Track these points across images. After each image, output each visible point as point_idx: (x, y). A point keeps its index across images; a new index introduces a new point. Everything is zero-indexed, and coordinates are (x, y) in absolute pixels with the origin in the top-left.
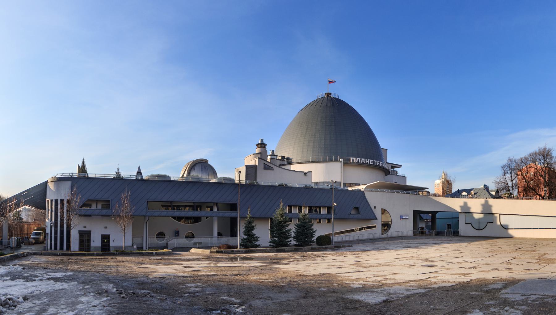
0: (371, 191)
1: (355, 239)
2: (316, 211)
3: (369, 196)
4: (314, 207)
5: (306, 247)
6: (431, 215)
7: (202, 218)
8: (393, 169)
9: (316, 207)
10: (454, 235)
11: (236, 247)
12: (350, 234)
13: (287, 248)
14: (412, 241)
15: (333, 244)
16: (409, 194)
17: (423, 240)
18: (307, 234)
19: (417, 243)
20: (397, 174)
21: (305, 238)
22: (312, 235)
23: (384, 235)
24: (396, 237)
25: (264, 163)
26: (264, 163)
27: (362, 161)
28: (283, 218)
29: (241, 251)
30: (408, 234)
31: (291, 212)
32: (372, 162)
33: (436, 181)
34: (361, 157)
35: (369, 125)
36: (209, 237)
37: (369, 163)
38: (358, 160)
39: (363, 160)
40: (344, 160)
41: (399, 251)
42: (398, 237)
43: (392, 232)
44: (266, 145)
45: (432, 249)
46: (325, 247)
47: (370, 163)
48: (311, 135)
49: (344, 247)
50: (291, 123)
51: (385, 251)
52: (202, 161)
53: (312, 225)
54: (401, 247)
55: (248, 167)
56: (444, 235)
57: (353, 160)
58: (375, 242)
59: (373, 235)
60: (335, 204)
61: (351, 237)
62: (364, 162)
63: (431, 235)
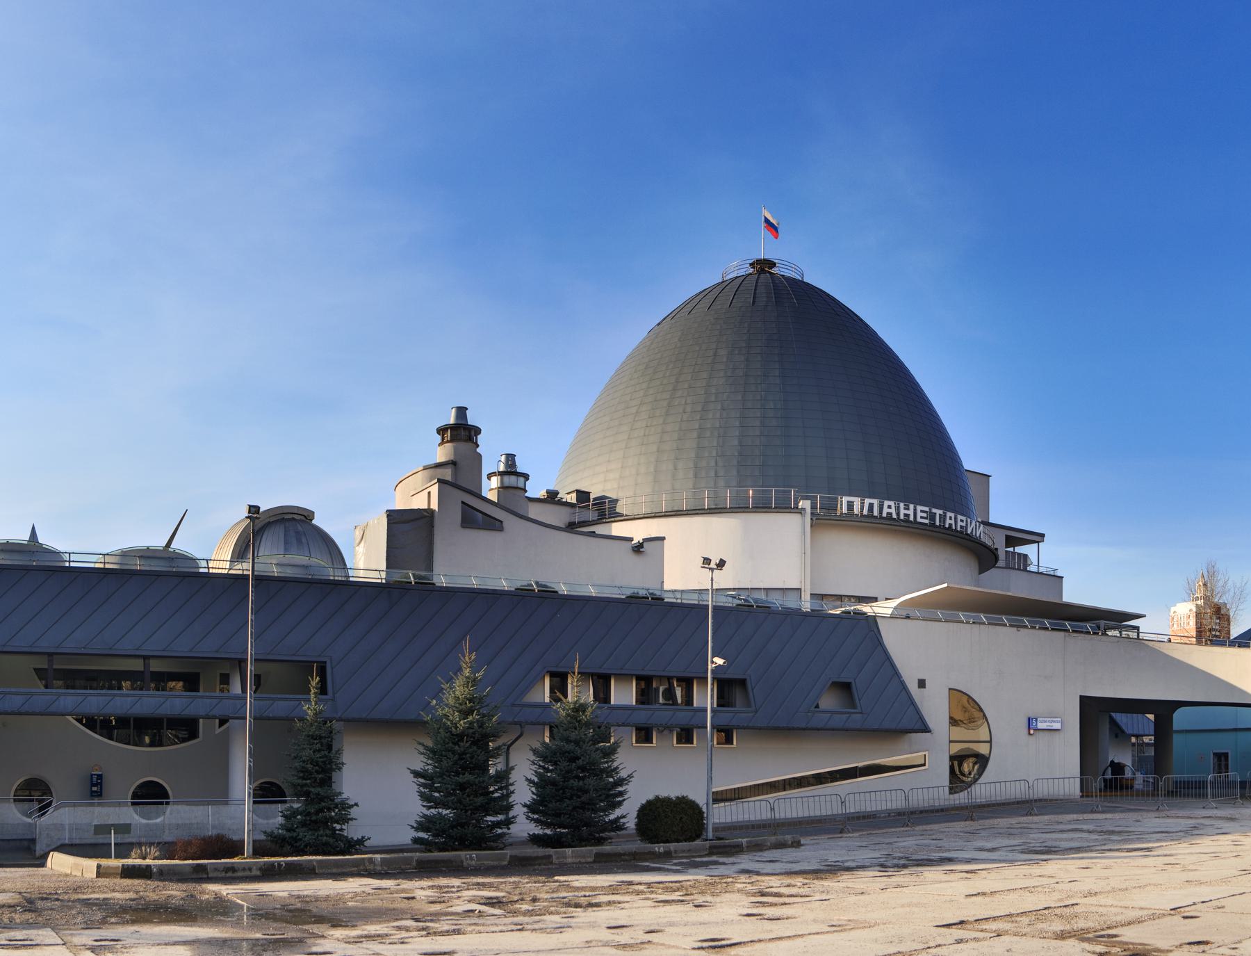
0: (908, 617)
1: (879, 808)
2: (669, 694)
3: (896, 640)
4: (660, 678)
5: (569, 851)
6: (1151, 717)
7: (201, 720)
8: (1011, 549)
9: (669, 679)
10: (1243, 797)
11: (233, 848)
12: (816, 793)
13: (474, 854)
14: (1070, 822)
15: (710, 835)
16: (1062, 634)
17: (1117, 816)
18: (586, 792)
19: (1091, 827)
20: (1026, 565)
21: (574, 808)
22: (612, 796)
23: (956, 796)
24: (1009, 804)
25: (463, 502)
26: (463, 502)
27: (886, 510)
28: (470, 718)
29: (244, 869)
30: (1051, 792)
31: (607, 699)
32: (925, 515)
33: (1175, 606)
34: (882, 497)
35: (907, 364)
36: (208, 804)
37: (912, 518)
38: (871, 505)
39: (890, 508)
40: (813, 507)
41: (993, 875)
42: (1018, 803)
43: (984, 790)
44: (477, 431)
45: (1150, 861)
46: (662, 850)
47: (919, 520)
48: (689, 409)
49: (758, 847)
50: (618, 370)
51: (931, 874)
52: (291, 516)
53: (610, 752)
54: (1012, 849)
55: (396, 519)
56: (1204, 796)
57: (850, 505)
58: (914, 824)
59: (907, 799)
60: (719, 661)
61: (811, 805)
62: (894, 516)
63: (1148, 795)
